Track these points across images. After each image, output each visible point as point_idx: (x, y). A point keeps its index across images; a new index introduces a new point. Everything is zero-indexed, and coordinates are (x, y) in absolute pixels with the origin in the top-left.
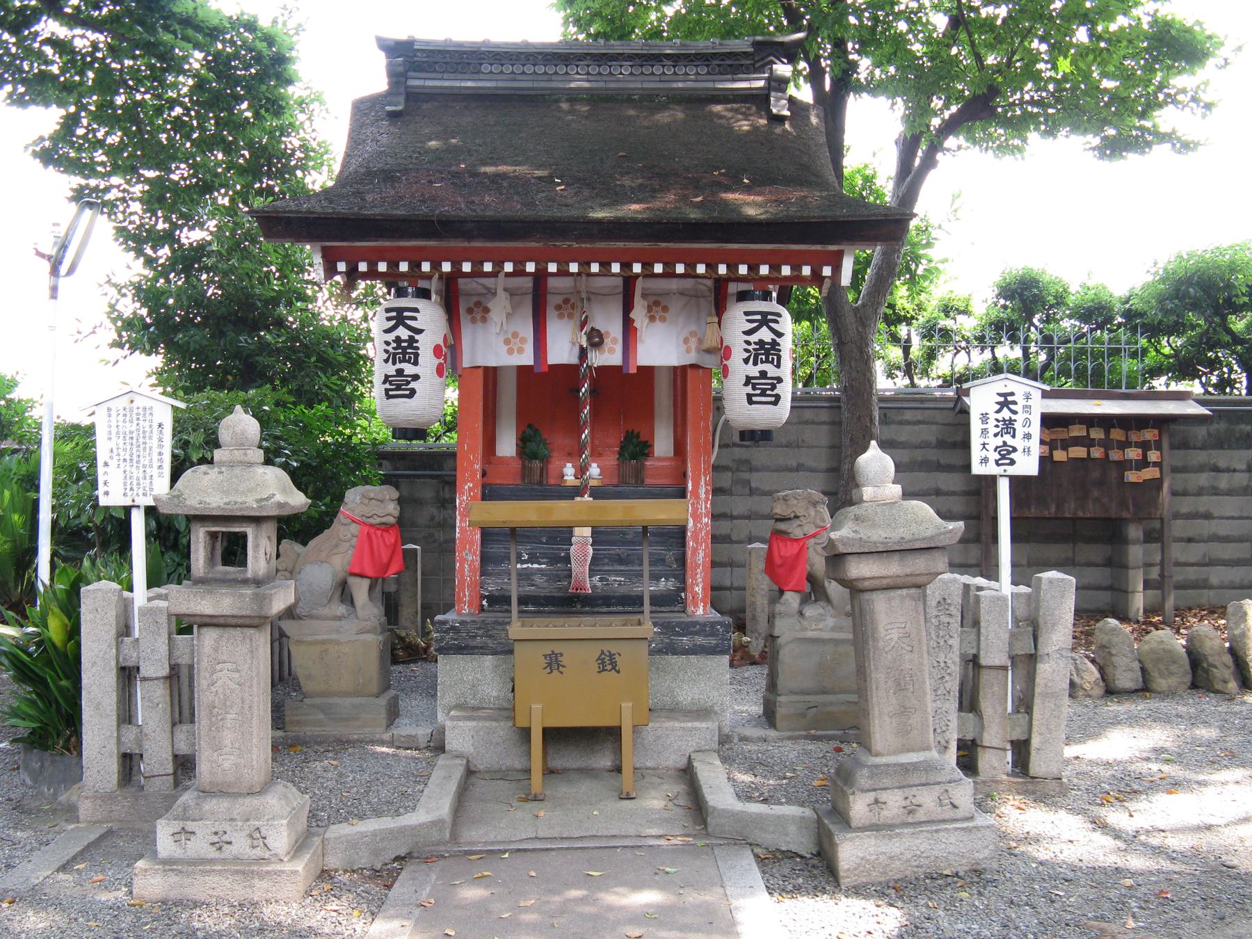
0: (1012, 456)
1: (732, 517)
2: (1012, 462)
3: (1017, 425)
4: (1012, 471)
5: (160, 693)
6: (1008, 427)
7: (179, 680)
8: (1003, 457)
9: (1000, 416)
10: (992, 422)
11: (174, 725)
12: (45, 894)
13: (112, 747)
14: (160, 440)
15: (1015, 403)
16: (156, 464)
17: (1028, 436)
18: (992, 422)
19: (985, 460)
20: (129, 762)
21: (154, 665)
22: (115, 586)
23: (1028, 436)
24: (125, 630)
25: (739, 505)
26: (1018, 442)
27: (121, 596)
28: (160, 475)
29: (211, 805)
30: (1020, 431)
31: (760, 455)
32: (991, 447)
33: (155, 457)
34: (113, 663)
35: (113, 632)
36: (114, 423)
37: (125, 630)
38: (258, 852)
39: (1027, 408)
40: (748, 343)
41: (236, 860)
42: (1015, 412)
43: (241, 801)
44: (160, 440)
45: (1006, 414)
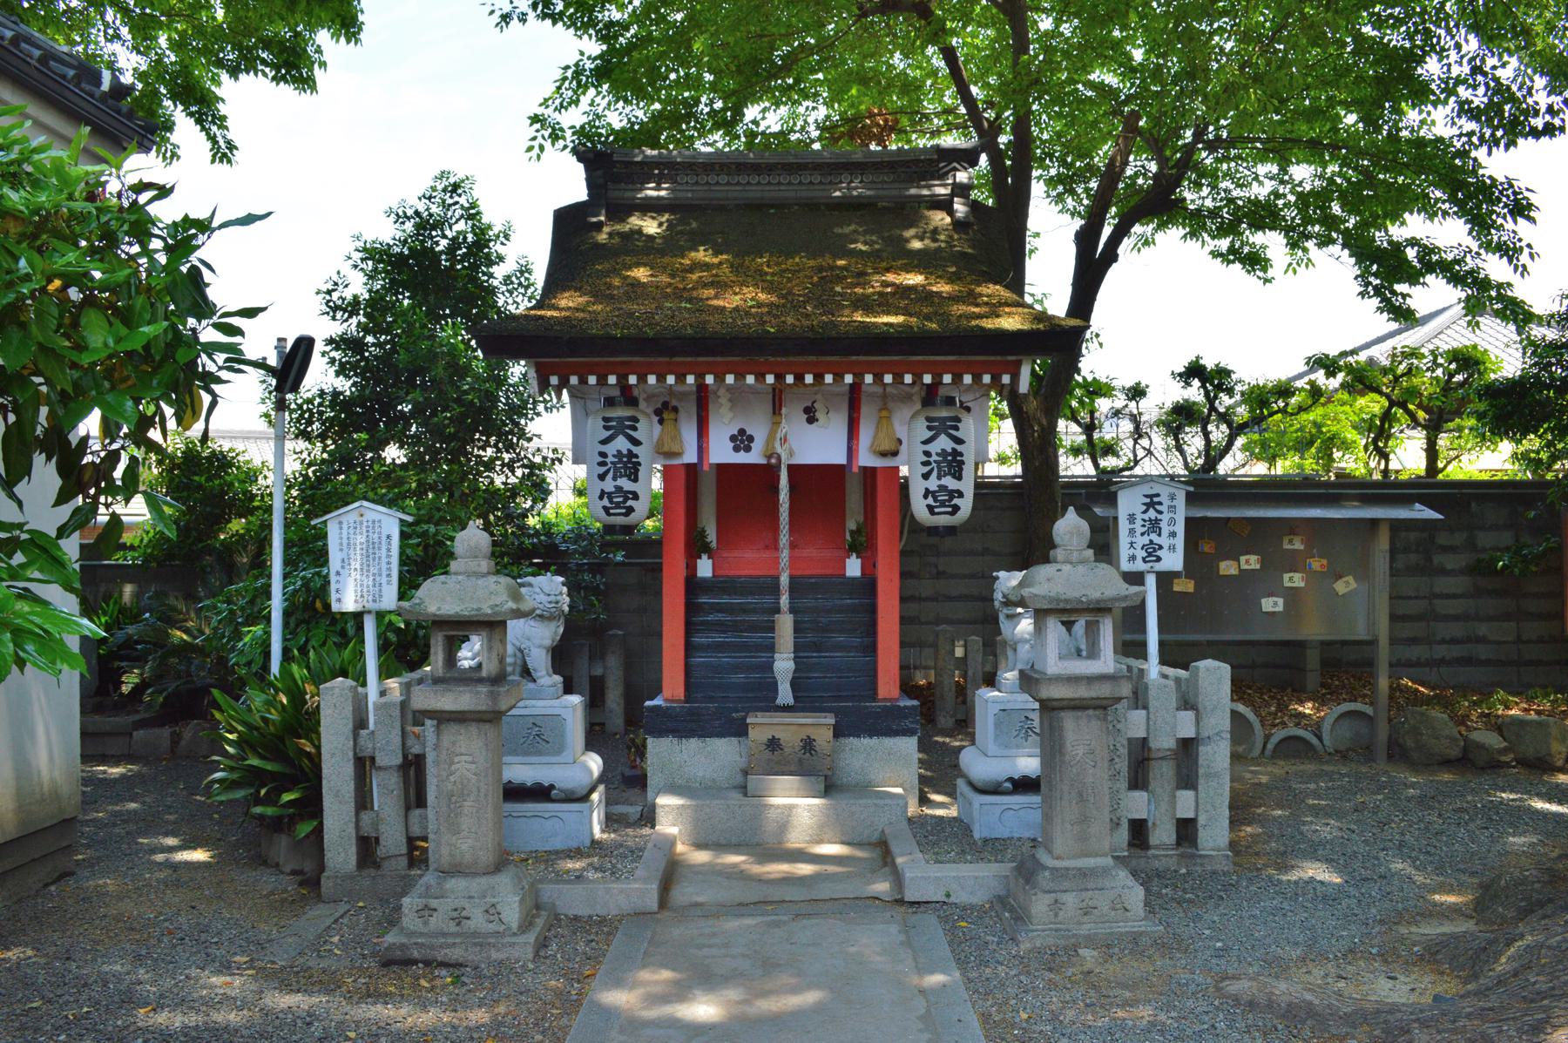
0: (1159, 553)
1: (921, 599)
2: (1159, 559)
3: (1163, 525)
4: (1159, 567)
5: (394, 781)
6: (1154, 526)
7: (413, 768)
8: (1150, 555)
9: (1146, 517)
10: (1139, 522)
11: (408, 808)
12: (1059, 115)
13: (351, 830)
14: (389, 550)
15: (1160, 503)
16: (384, 573)
17: (1173, 534)
18: (1139, 522)
19: (1133, 558)
20: (367, 847)
21: (389, 756)
22: (350, 682)
23: (1173, 534)
24: (360, 723)
25: (926, 587)
26: (1164, 540)
27: (356, 693)
28: (389, 583)
29: (452, 884)
30: (1165, 532)
31: (948, 542)
32: (1138, 546)
33: (384, 566)
34: (351, 754)
35: (351, 726)
36: (345, 535)
37: (360, 723)
38: (492, 927)
39: (1172, 509)
40: (927, 454)
41: (475, 934)
42: (1161, 513)
43: (478, 880)
44: (389, 550)
45: (1152, 514)
